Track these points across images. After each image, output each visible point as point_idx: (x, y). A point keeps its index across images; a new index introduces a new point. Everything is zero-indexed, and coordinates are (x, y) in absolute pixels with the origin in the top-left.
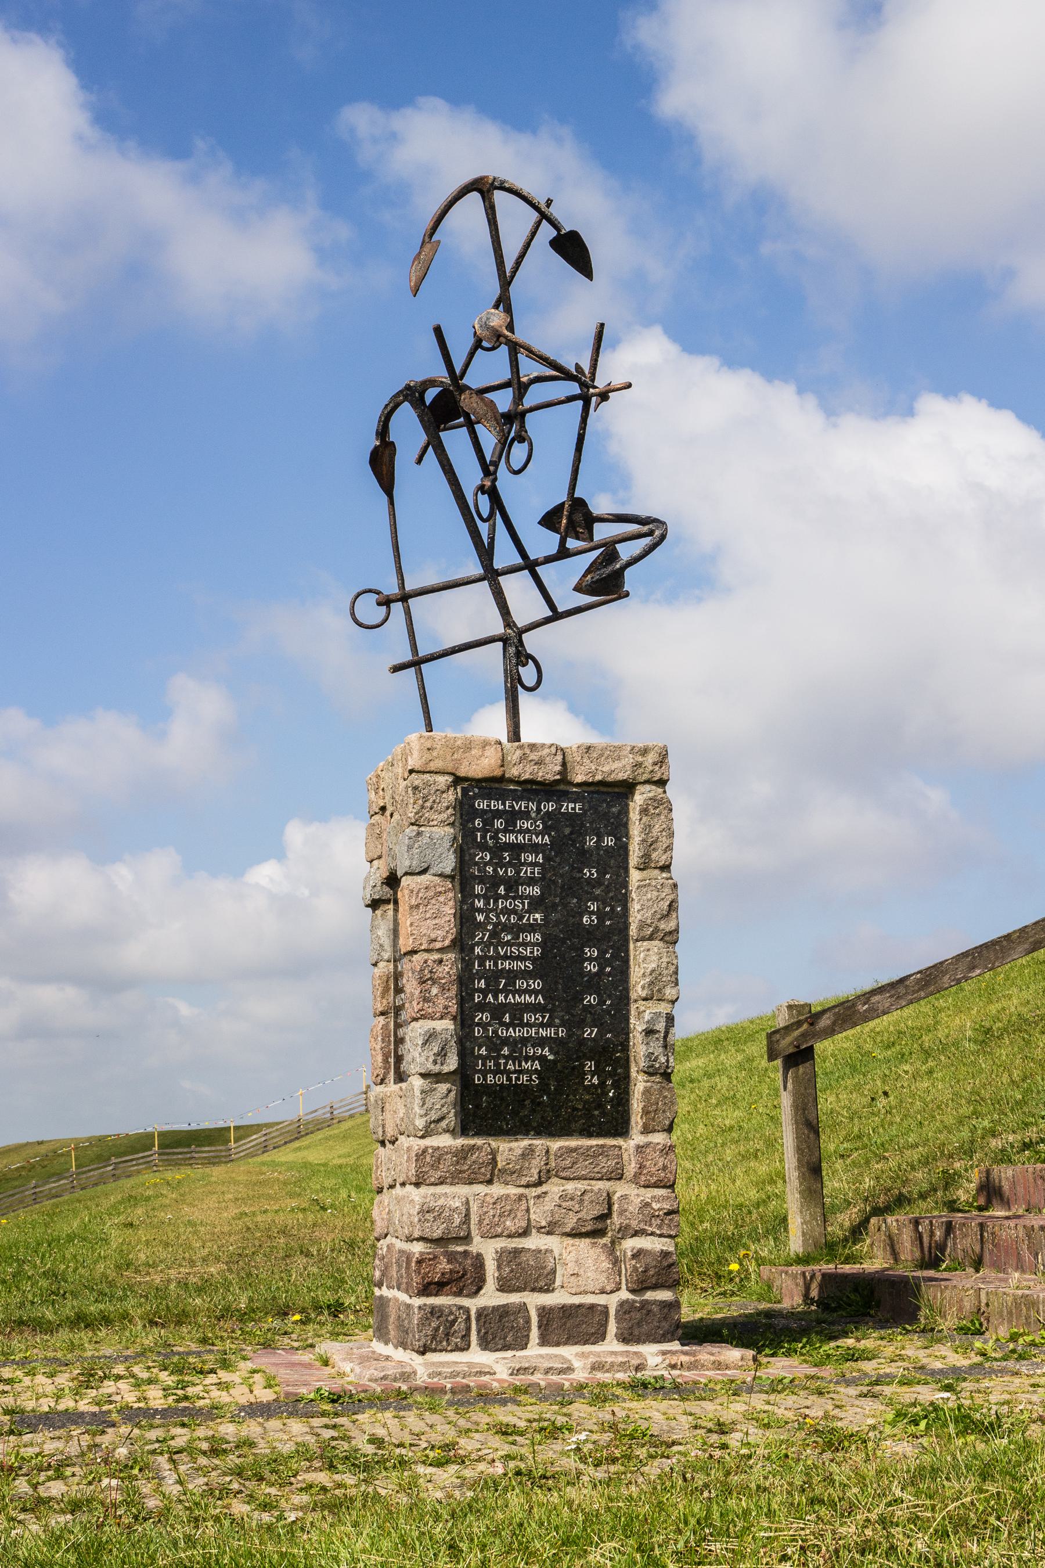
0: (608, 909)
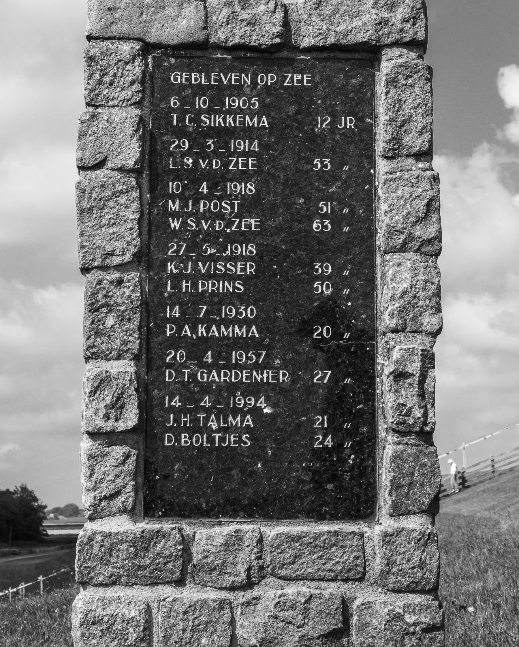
0: (346, 211)
